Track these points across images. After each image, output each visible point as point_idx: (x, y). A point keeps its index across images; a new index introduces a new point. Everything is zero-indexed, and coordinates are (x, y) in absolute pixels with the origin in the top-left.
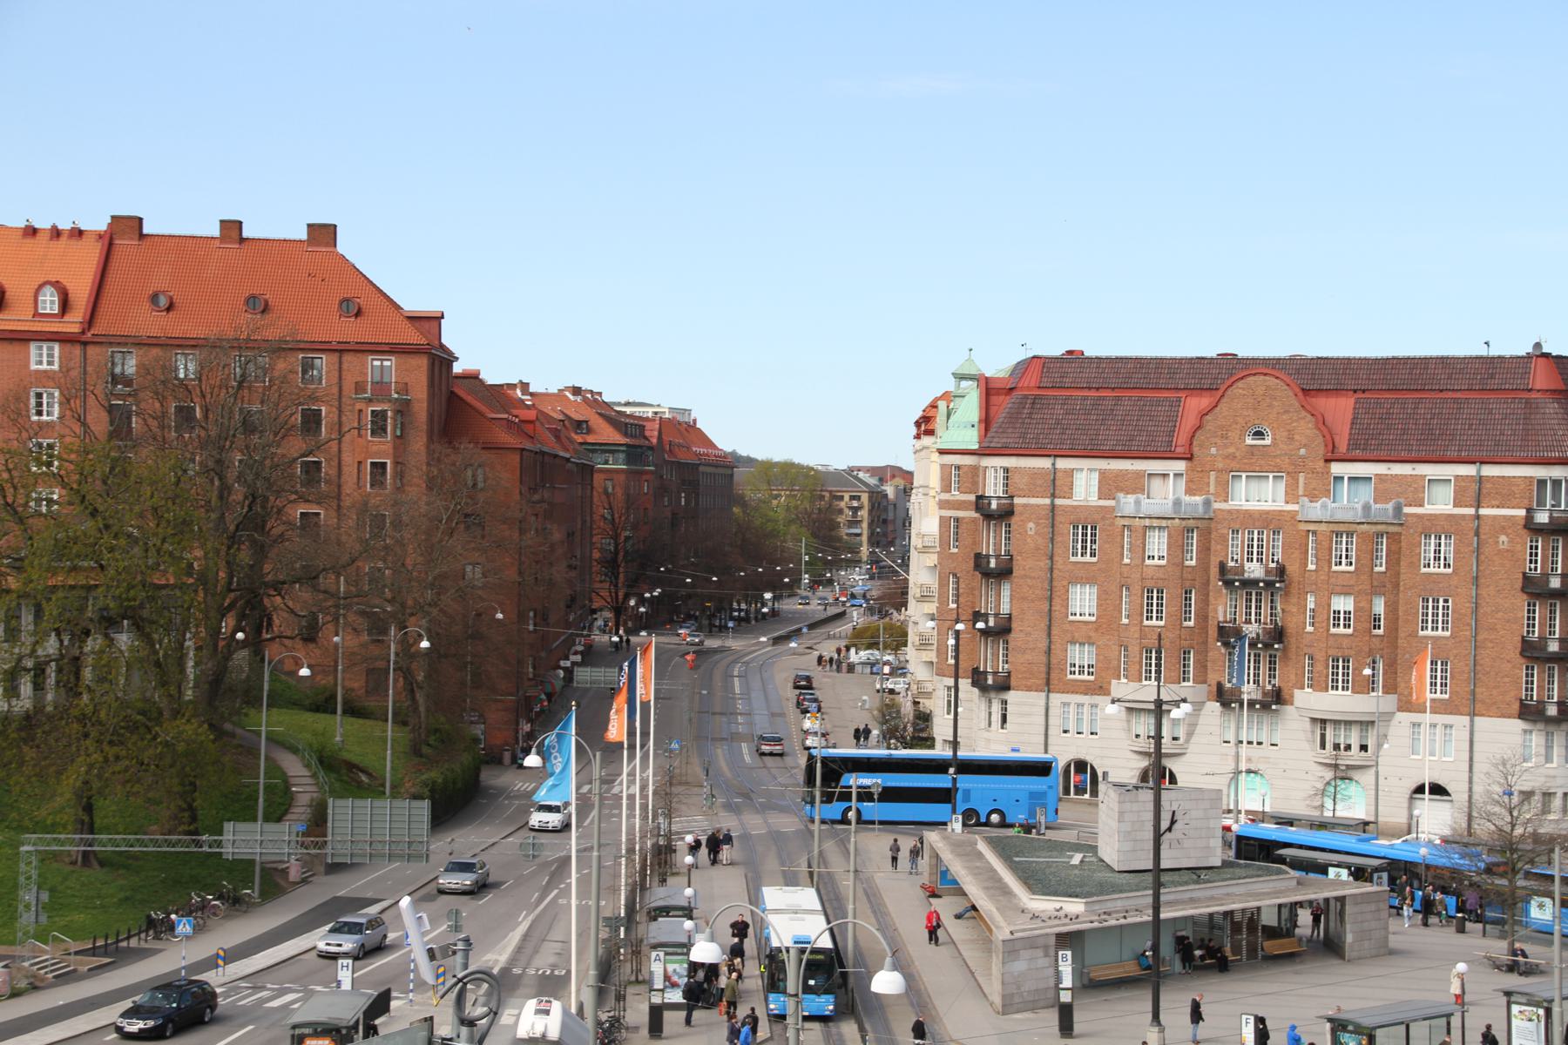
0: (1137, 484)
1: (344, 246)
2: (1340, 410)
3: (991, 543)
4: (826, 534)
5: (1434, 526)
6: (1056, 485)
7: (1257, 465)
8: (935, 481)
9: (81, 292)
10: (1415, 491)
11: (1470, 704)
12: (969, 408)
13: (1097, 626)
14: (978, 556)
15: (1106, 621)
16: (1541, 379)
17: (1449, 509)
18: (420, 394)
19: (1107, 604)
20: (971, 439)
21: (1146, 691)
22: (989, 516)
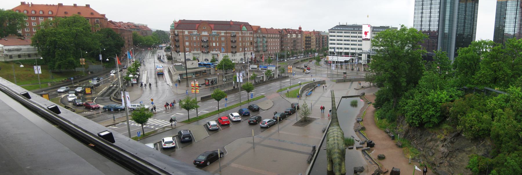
1: (91, 7)
5: (223, 36)
6: (183, 32)
7: (204, 30)
10: (220, 33)
19: (190, 44)
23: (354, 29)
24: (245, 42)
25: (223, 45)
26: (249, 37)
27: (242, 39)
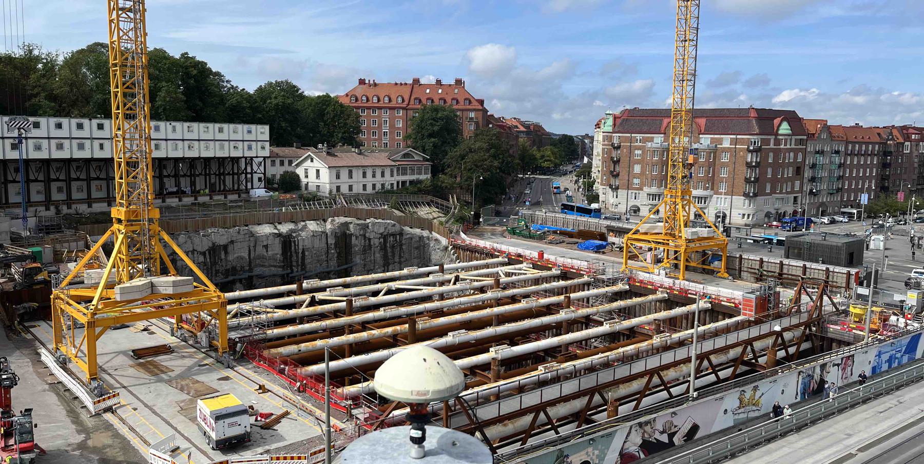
0: (652, 140)
2: (702, 121)
3: (614, 154)
4: (571, 150)
5: (725, 150)
8: (601, 138)
9: (406, 98)
10: (720, 141)
11: (731, 192)
12: (610, 122)
13: (640, 174)
14: (747, 163)
15: (643, 172)
16: (753, 114)
17: (728, 146)
18: (480, 120)
20: (610, 129)
21: (654, 190)
22: (614, 148)
23: (350, 302)
24: (784, 166)
25: (724, 174)
26: (796, 151)
27: (776, 158)
